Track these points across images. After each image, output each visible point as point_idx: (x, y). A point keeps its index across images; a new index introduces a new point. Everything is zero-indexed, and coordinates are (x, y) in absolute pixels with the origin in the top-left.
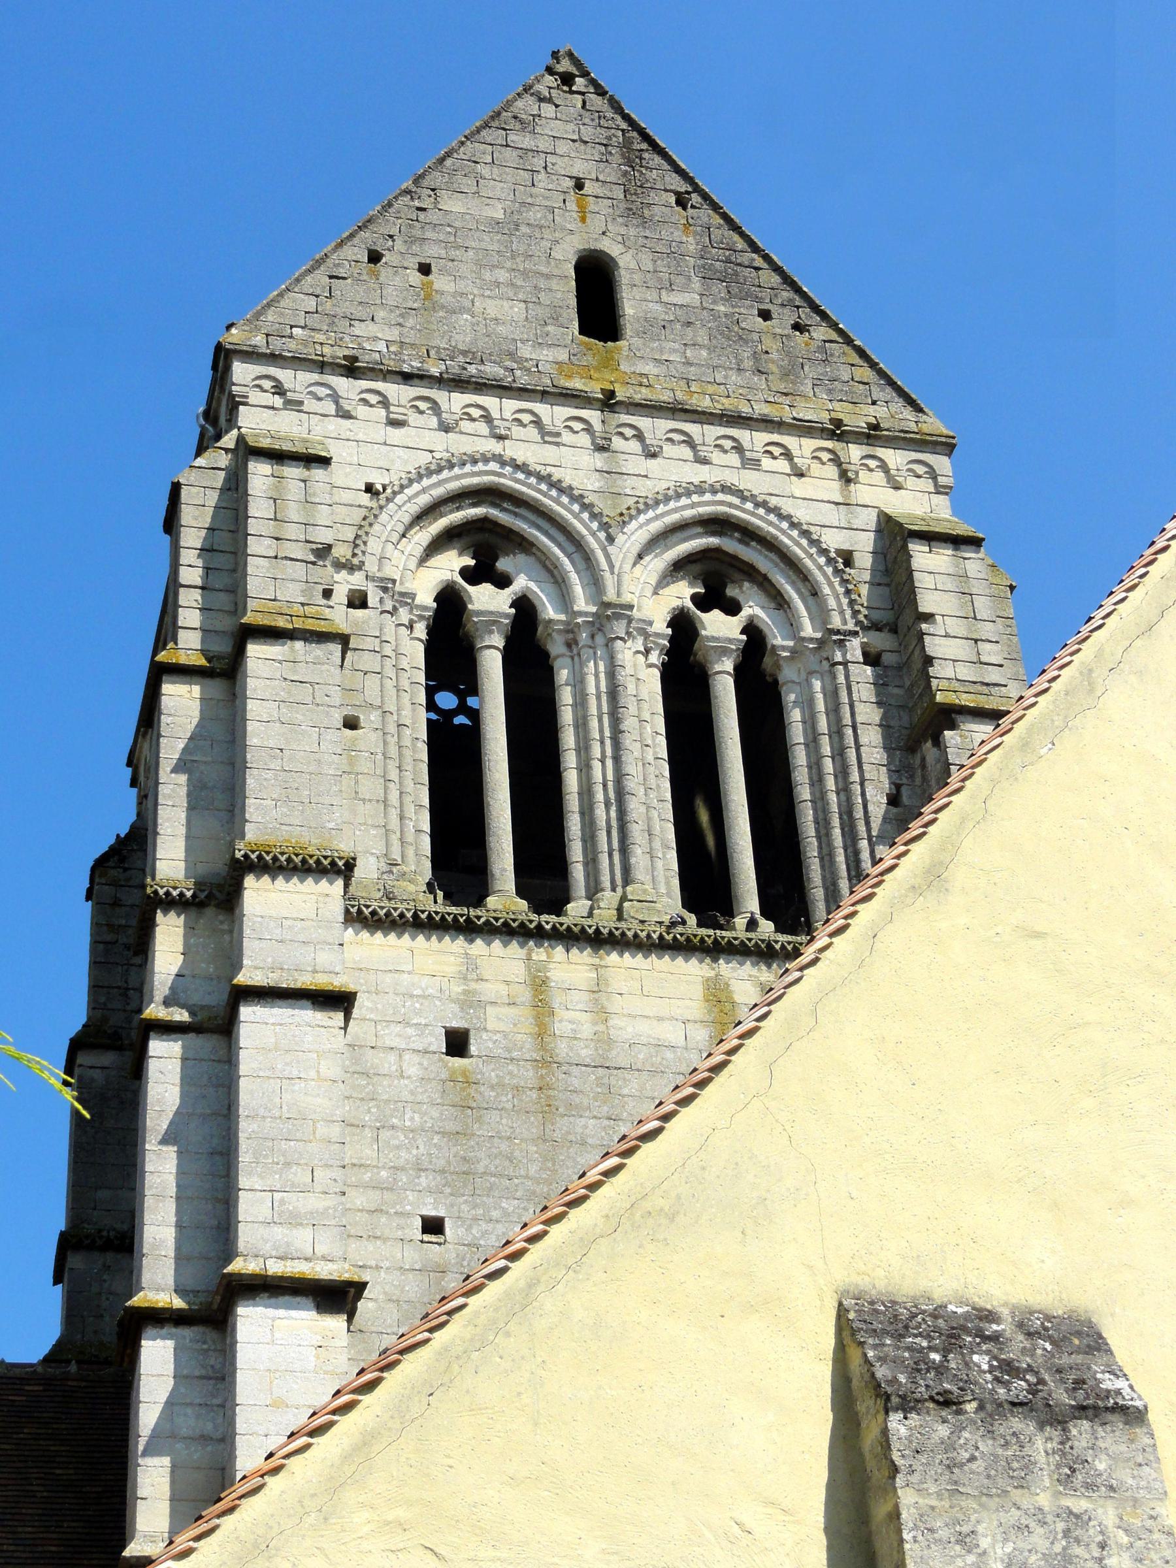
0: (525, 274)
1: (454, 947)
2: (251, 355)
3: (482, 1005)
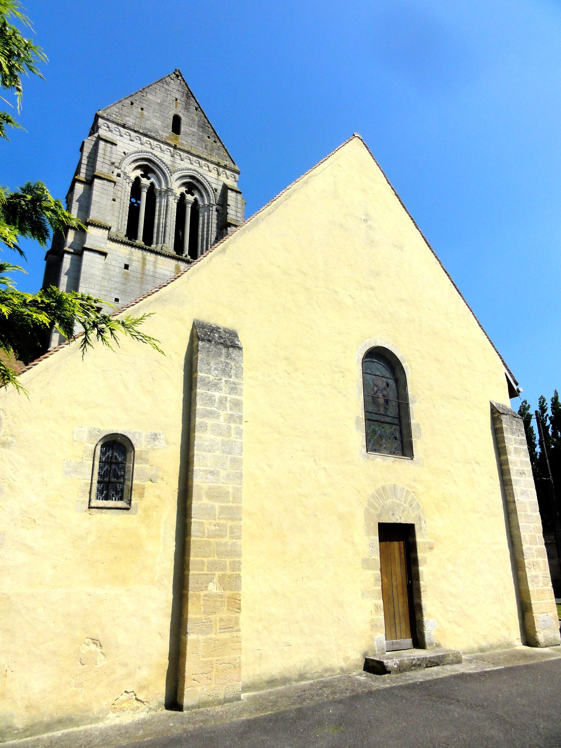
0: (163, 116)
1: (129, 248)
2: (103, 118)
3: (132, 261)
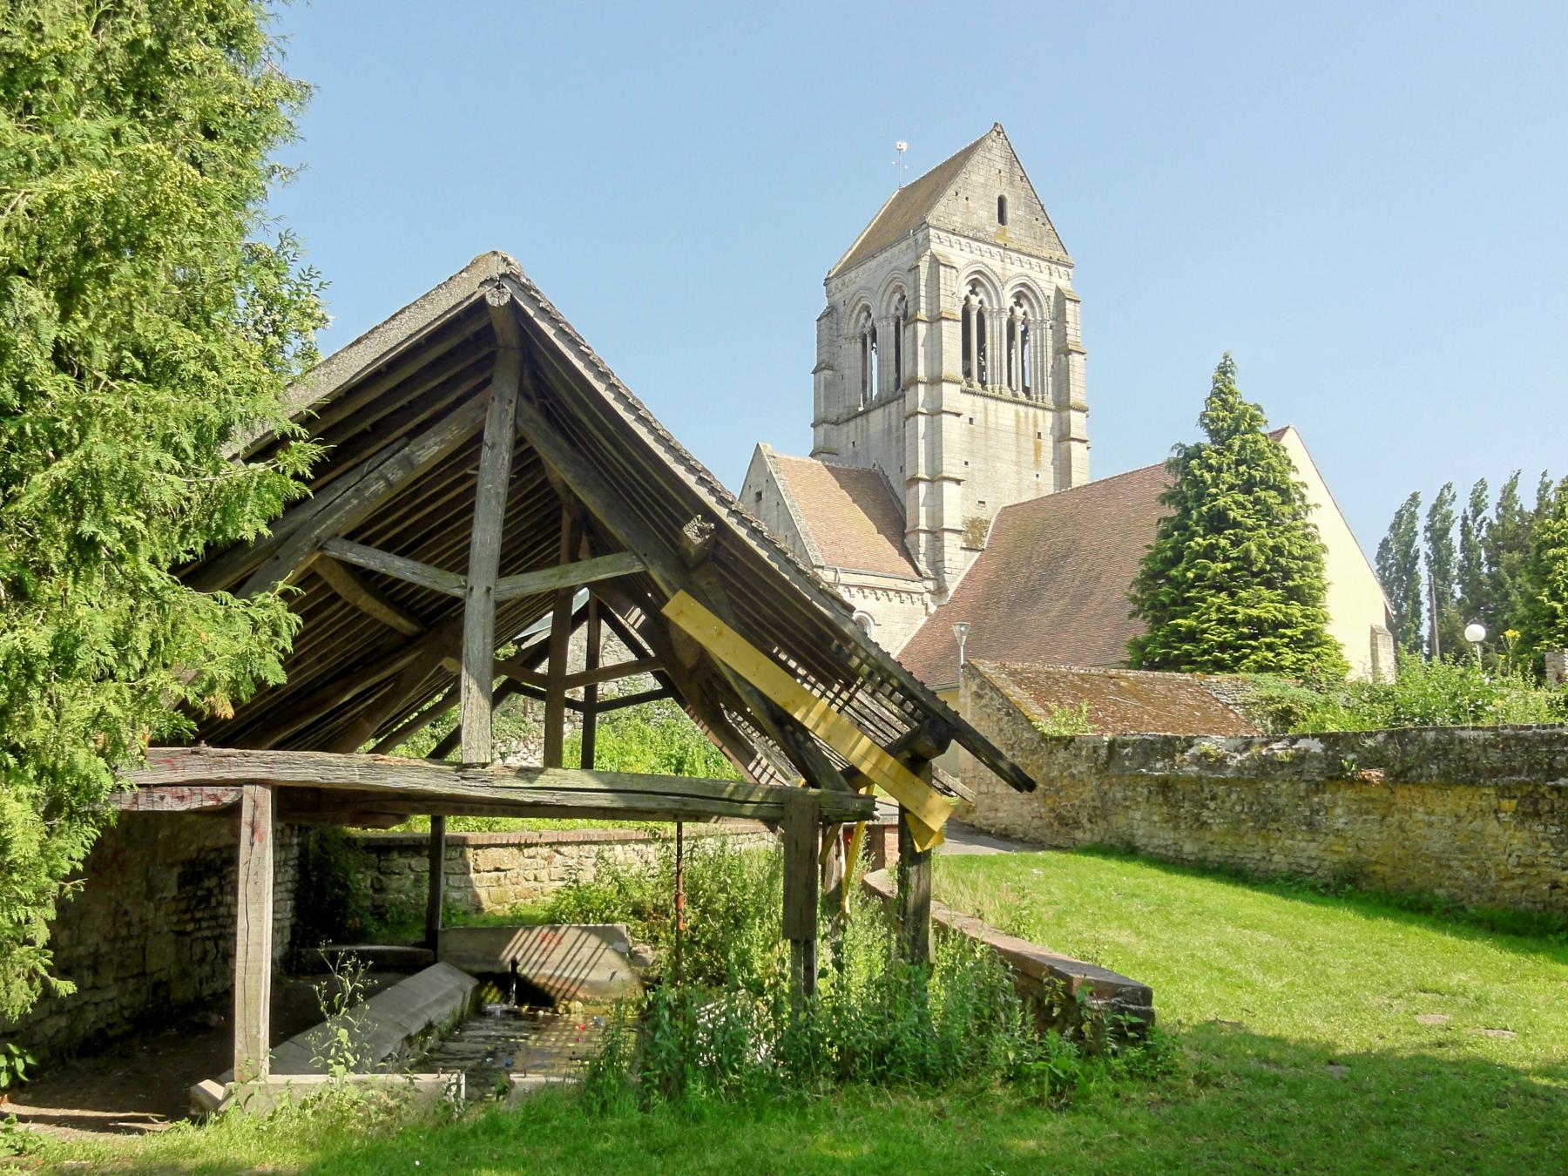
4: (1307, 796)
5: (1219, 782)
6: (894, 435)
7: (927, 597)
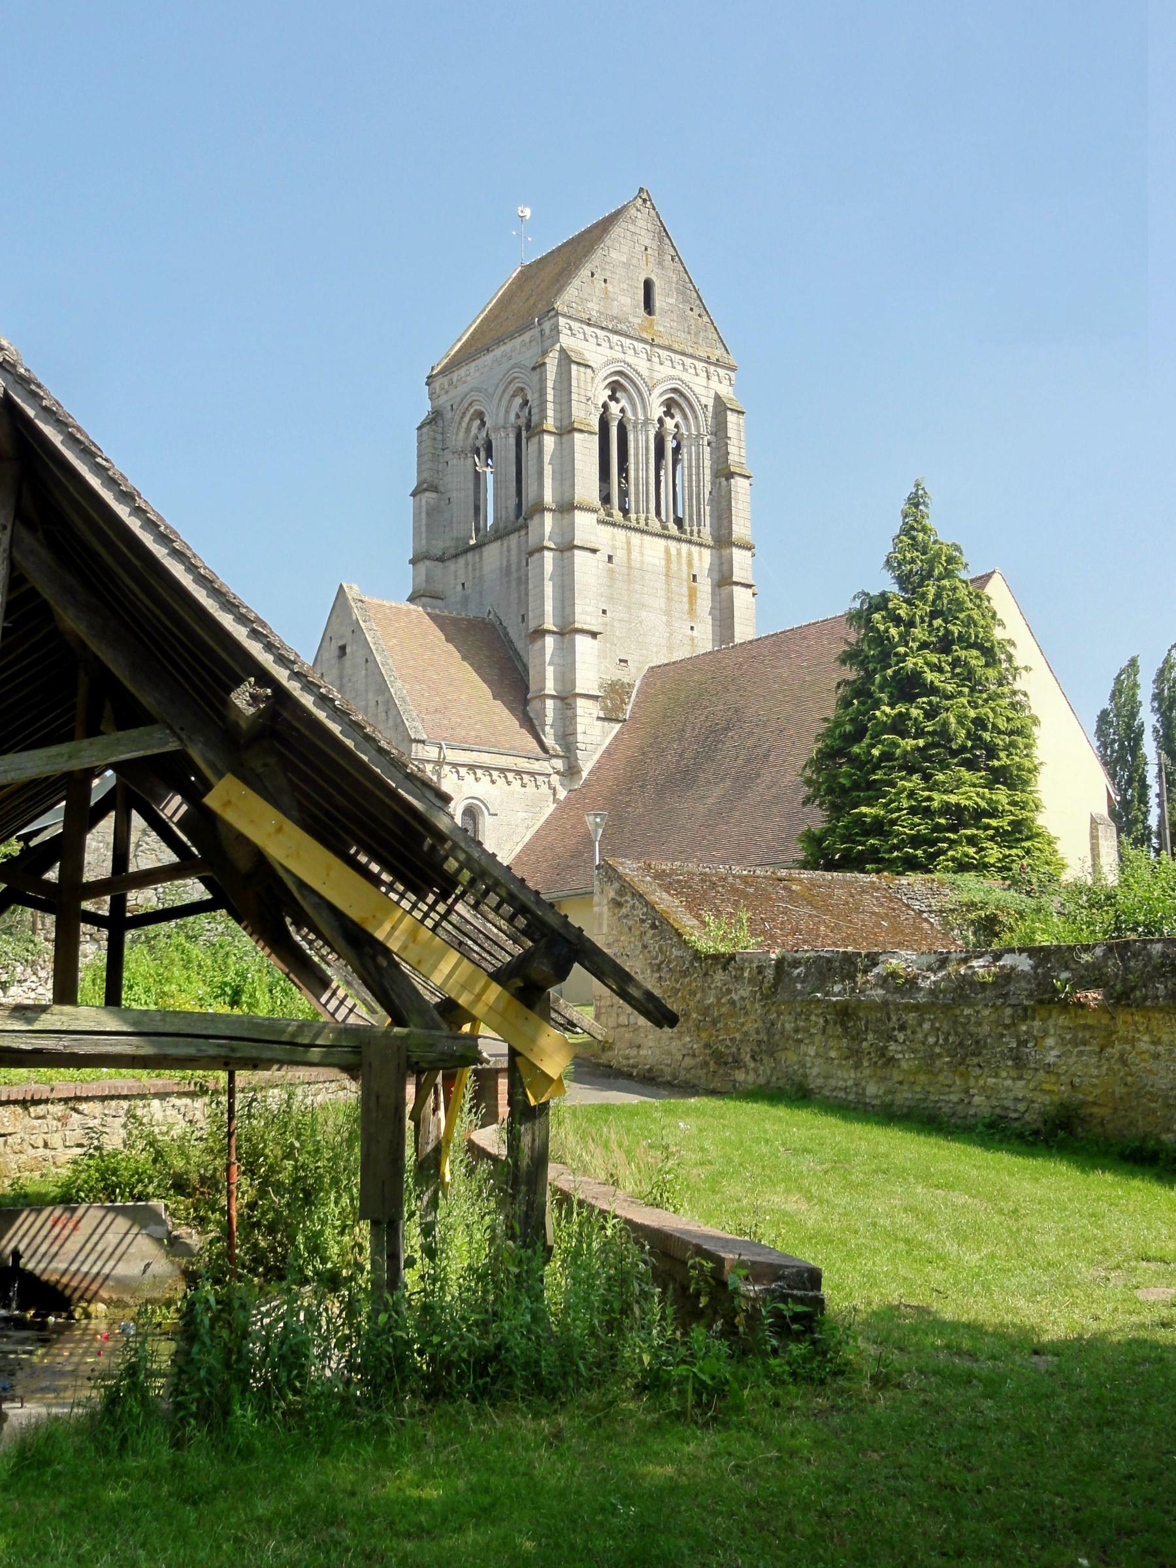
1: (610, 529)
2: (564, 316)
4: (1014, 1024)
5: (909, 1008)
6: (514, 576)
7: (555, 779)
